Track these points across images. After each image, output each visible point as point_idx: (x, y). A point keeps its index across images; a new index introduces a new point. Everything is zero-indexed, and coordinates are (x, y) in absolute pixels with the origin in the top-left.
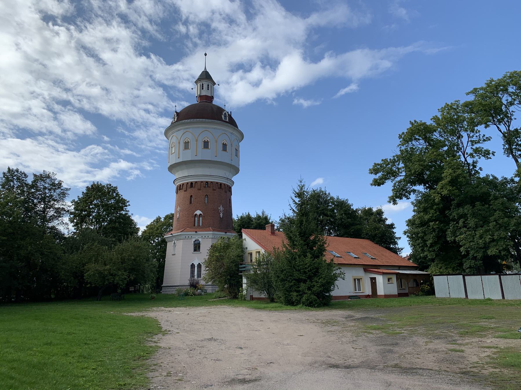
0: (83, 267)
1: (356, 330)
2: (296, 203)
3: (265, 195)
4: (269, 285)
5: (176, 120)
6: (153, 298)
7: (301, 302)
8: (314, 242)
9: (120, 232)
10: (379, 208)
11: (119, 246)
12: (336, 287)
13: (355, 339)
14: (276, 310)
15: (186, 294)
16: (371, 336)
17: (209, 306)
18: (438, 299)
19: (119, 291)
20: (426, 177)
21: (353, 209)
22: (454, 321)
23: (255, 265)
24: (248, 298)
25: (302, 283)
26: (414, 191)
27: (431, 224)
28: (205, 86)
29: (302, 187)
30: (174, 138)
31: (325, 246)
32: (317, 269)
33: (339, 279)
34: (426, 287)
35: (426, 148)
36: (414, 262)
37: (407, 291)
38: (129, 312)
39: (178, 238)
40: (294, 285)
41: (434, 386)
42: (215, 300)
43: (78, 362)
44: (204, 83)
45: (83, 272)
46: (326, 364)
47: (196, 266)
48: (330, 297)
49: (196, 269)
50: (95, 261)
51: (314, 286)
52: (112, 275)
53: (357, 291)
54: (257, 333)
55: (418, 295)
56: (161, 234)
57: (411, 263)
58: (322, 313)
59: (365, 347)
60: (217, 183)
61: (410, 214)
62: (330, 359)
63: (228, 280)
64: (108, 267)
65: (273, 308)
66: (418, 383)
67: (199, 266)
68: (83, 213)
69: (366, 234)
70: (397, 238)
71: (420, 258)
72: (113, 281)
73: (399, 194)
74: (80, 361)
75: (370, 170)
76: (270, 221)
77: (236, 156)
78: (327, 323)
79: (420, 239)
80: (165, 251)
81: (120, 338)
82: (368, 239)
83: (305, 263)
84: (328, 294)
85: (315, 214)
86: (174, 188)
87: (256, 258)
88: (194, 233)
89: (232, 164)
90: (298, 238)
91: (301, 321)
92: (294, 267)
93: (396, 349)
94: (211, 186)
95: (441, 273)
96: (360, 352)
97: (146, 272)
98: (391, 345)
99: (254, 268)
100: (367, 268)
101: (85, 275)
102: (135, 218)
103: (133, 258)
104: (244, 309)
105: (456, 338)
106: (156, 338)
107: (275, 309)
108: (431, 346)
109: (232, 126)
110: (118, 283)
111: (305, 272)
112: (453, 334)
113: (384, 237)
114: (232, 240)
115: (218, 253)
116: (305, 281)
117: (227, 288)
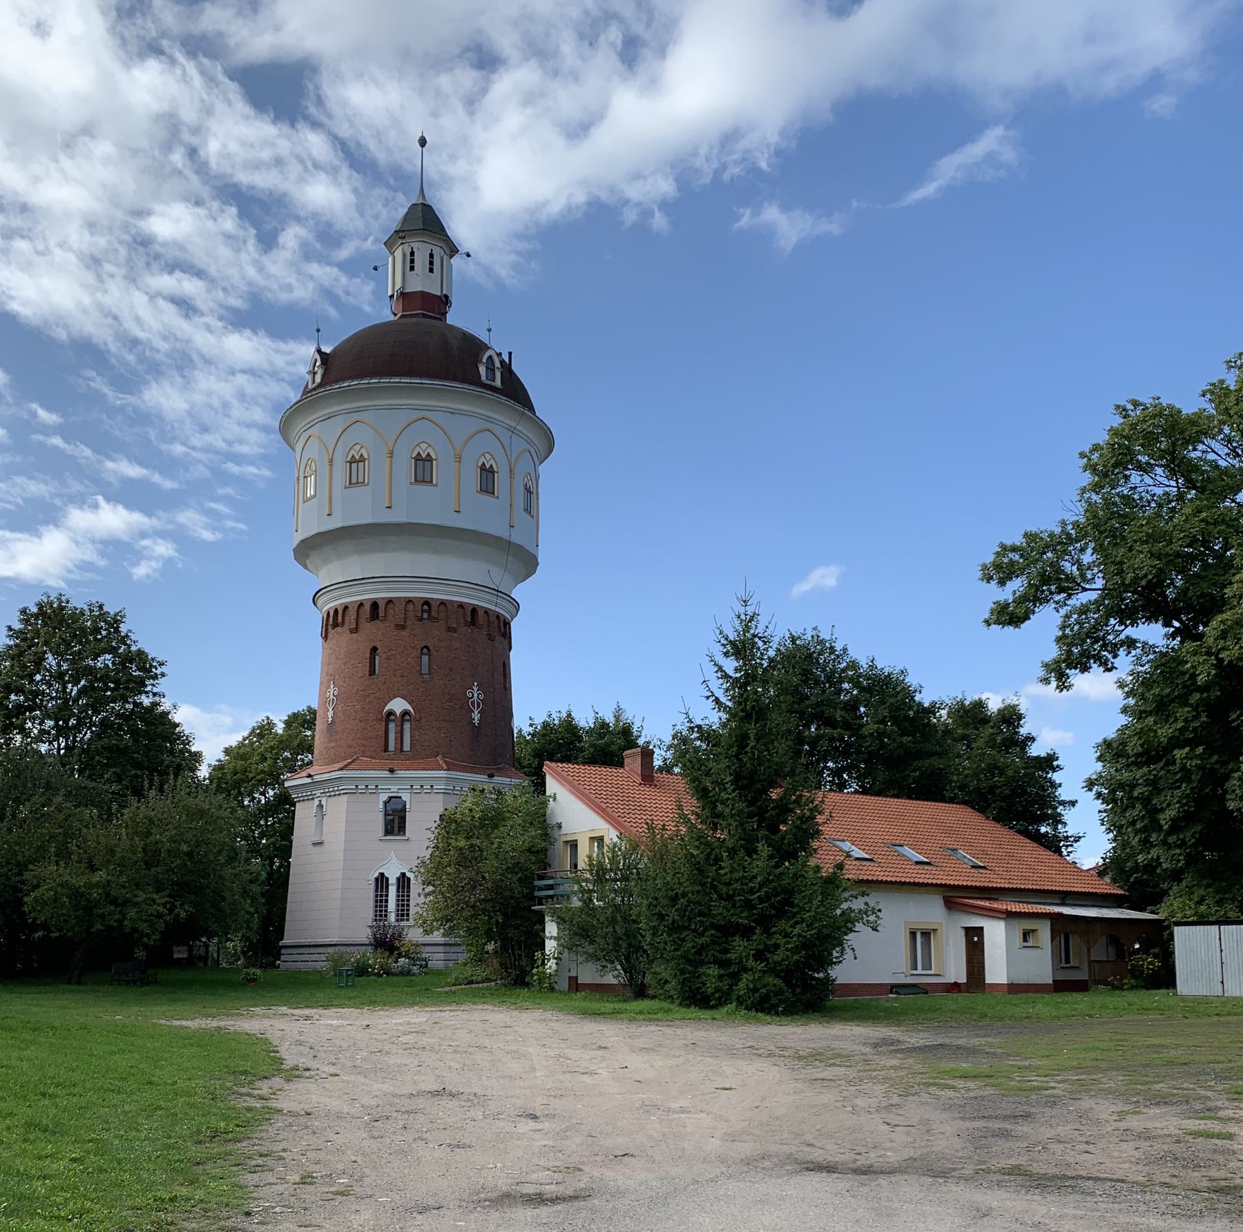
0: (20, 874)
1: (902, 1078)
2: (726, 676)
3: (620, 653)
4: (630, 945)
5: (318, 379)
6: (252, 980)
7: (734, 997)
8: (783, 808)
9: (138, 765)
10: (1013, 700)
11: (135, 810)
12: (848, 954)
13: (895, 1100)
14: (650, 1020)
15: (362, 971)
16: (950, 1093)
17: (435, 1005)
18: (1183, 999)
19: (140, 954)
20: (1170, 593)
21: (920, 704)
22: (1221, 1058)
23: (587, 880)
24: (564, 985)
25: (737, 938)
26: (1130, 643)
27: (1179, 754)
28: (421, 260)
29: (748, 622)
30: (314, 446)
31: (820, 819)
32: (790, 892)
33: (859, 926)
34: (1150, 963)
35: (1180, 497)
36: (1114, 880)
37: (1083, 975)
38: (172, 1017)
39: (331, 788)
40: (713, 942)
41: (1122, 1219)
42: (453, 988)
43: (25, 1141)
44: (416, 246)
45: (21, 891)
46: (796, 1161)
47: (392, 881)
48: (828, 981)
49: (392, 890)
50: (57, 855)
51: (777, 946)
52: (114, 902)
53: (919, 971)
54: (586, 1079)
55: (1121, 988)
56: (274, 778)
57: (1106, 886)
58: (800, 1030)
59: (925, 1122)
60: (461, 606)
61: (1112, 723)
62: (808, 1149)
63: (497, 923)
64: (101, 876)
65: (641, 1012)
66: (1074, 1212)
67: (403, 881)
68: (13, 697)
69: (962, 787)
70: (1063, 803)
71: (1136, 867)
72: (120, 922)
73: (1079, 652)
74: (32, 1137)
75: (984, 567)
76: (641, 742)
77: (528, 510)
78: (816, 1057)
79: (1139, 806)
80: (287, 831)
81: (150, 1083)
82: (965, 803)
83: (746, 872)
84: (821, 975)
85: (794, 719)
86: (315, 620)
87: (590, 857)
88: (386, 774)
89: (516, 539)
90: (730, 793)
91: (731, 1052)
92: (714, 888)
93: (1023, 1128)
94: (442, 616)
95: (1202, 916)
96: (908, 1134)
97: (227, 894)
98: (1006, 1118)
99: (583, 891)
100: (955, 897)
101: (26, 899)
102: (185, 716)
103: (185, 848)
104: (548, 1015)
105: (1219, 1104)
106: (264, 1088)
107: (650, 1017)
108: (1134, 1123)
109: (511, 403)
110: (135, 930)
111: (748, 904)
112: (1209, 1094)
113: (1017, 793)
114: (509, 799)
115: (462, 837)
116: (747, 932)
117: (496, 952)
